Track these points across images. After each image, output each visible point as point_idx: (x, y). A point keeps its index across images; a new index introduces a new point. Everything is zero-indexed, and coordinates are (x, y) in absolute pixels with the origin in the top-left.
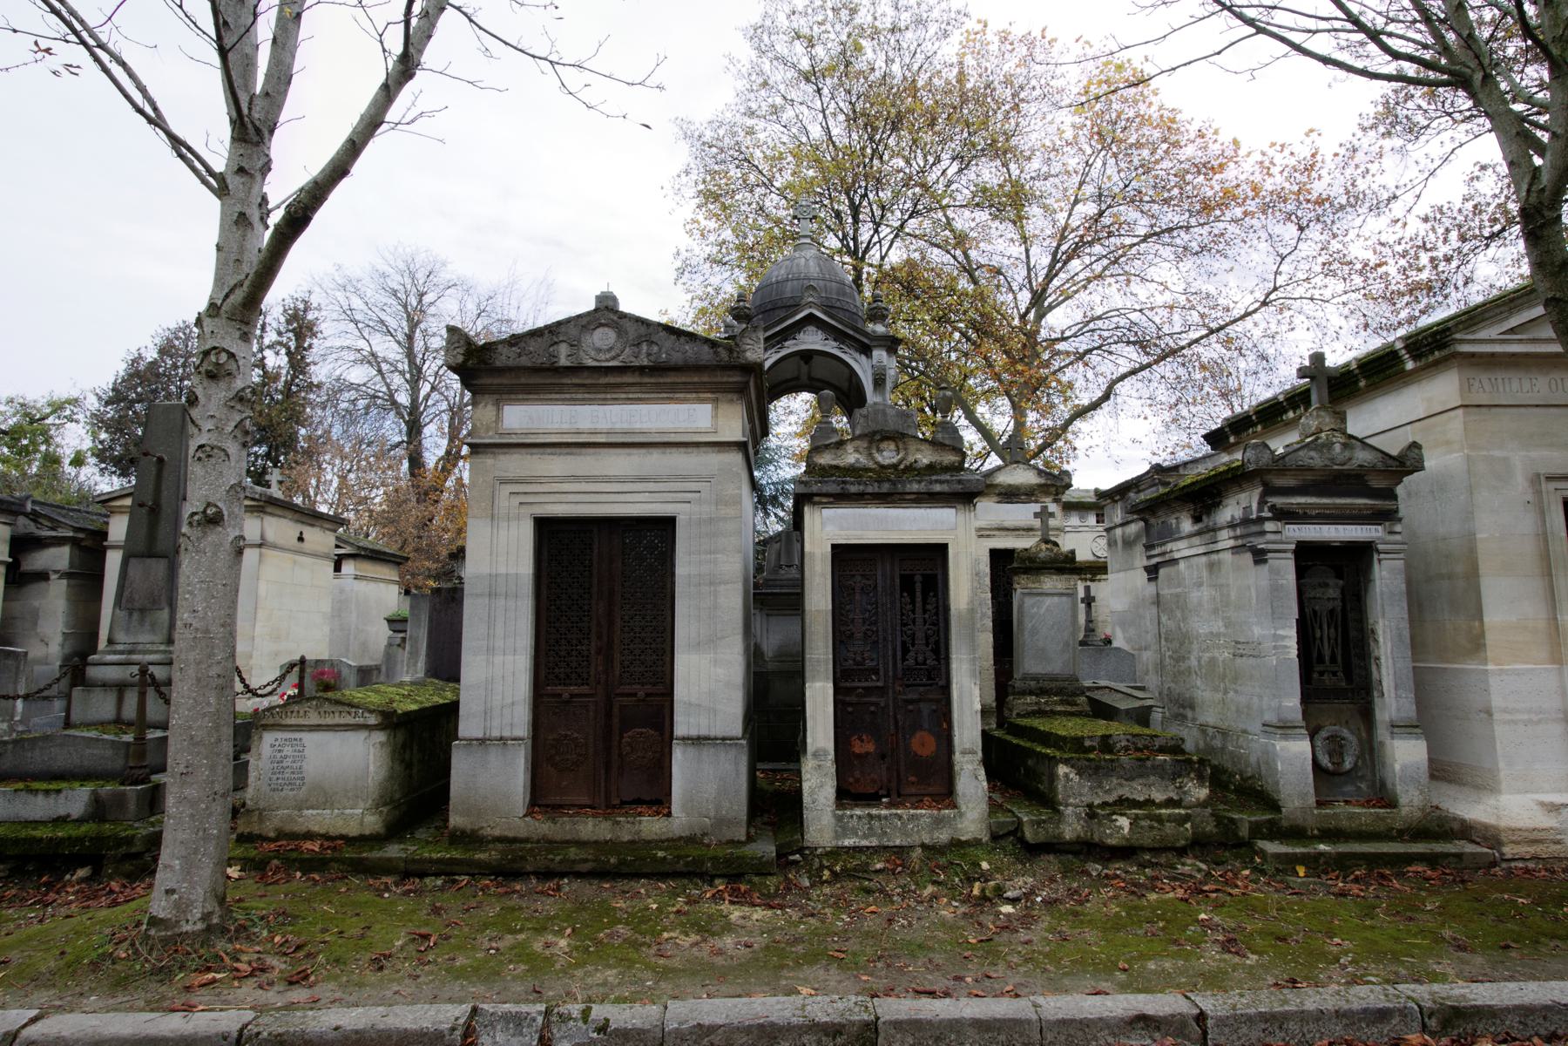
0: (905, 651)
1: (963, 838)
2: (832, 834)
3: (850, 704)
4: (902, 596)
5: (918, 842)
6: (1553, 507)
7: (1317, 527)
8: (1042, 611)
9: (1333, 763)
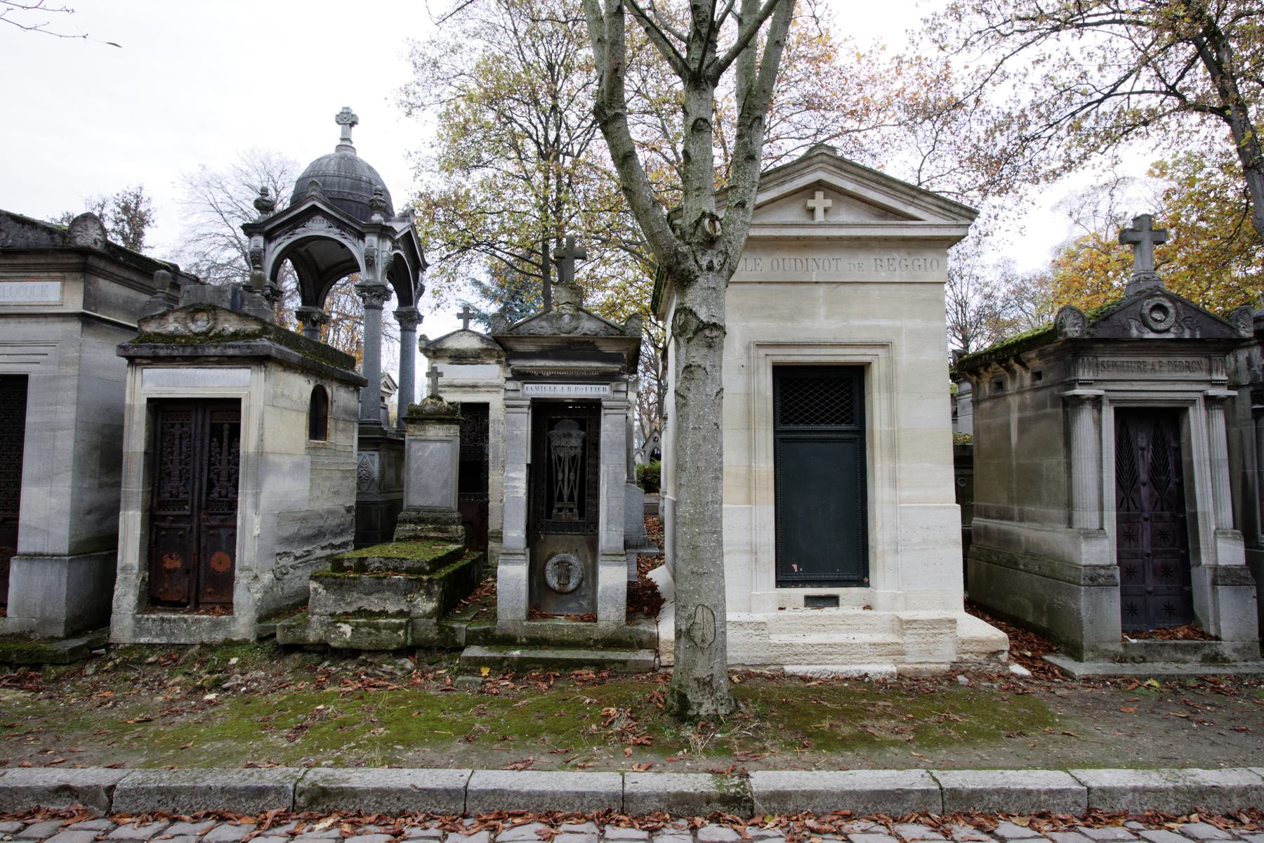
0: (211, 485)
1: (235, 639)
2: (131, 633)
3: (163, 529)
4: (211, 441)
5: (198, 641)
6: (762, 370)
7: (552, 386)
9: (560, 584)
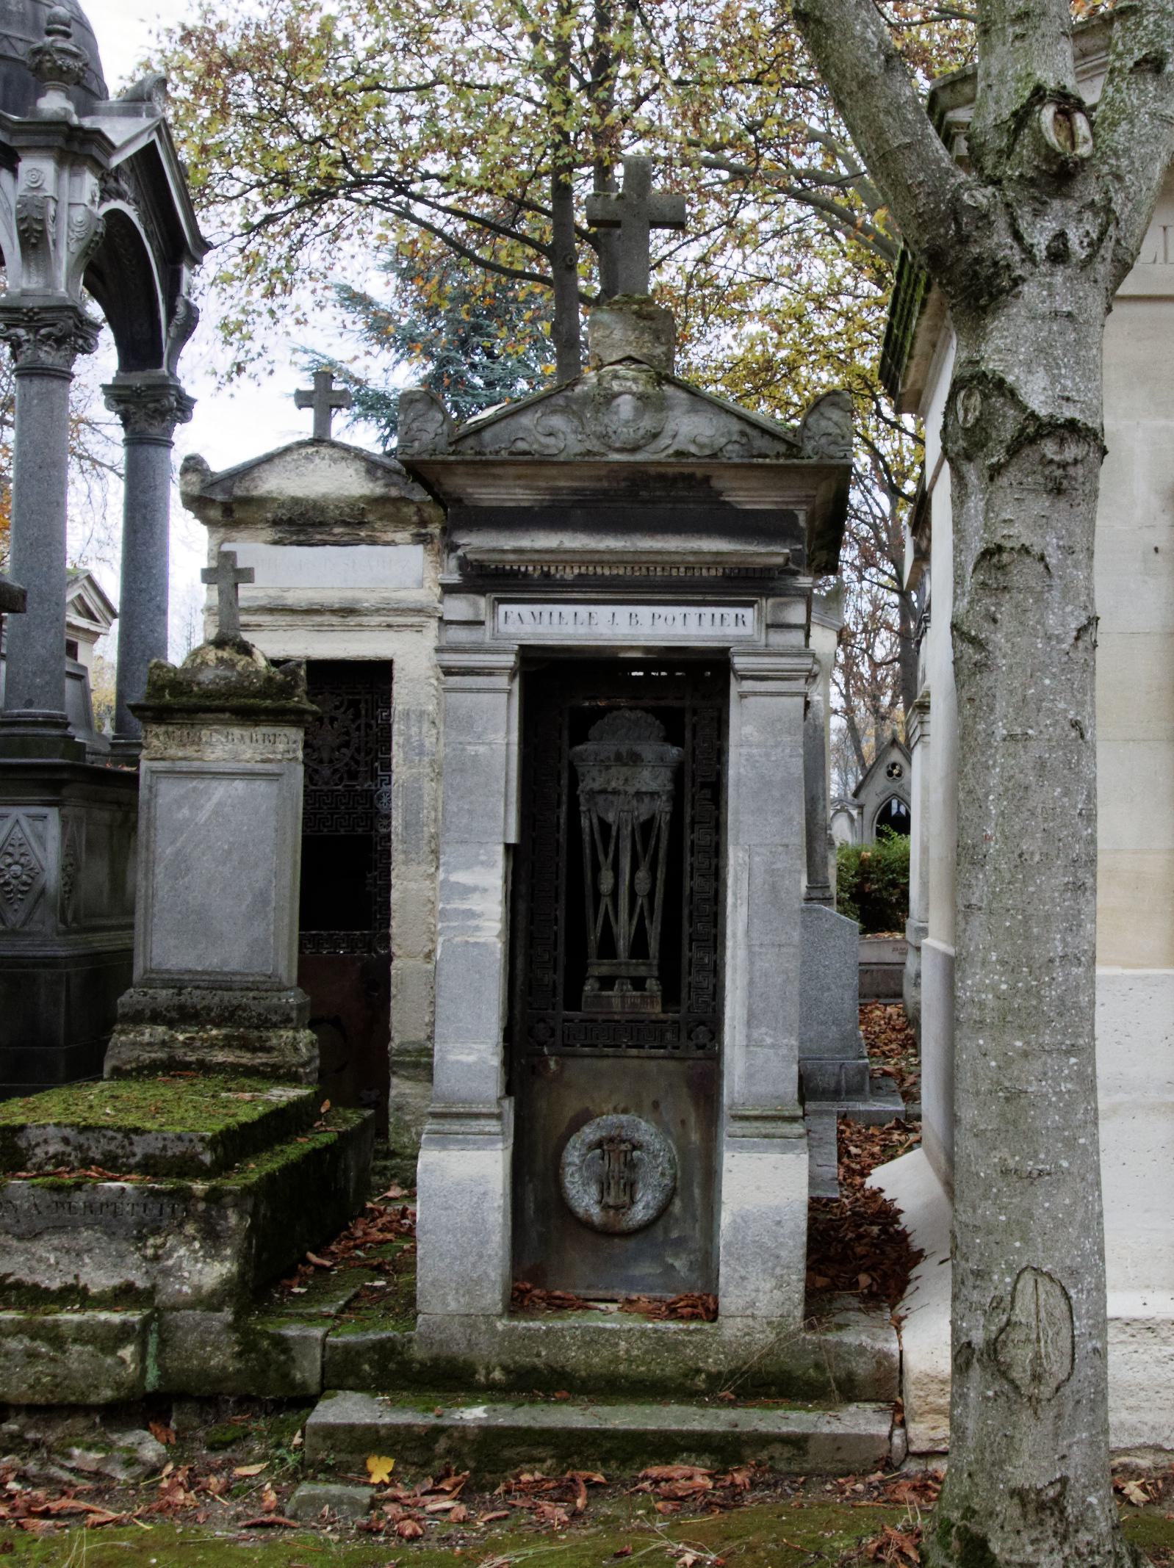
7: (583, 610)
8: (203, 816)
9: (606, 1207)
